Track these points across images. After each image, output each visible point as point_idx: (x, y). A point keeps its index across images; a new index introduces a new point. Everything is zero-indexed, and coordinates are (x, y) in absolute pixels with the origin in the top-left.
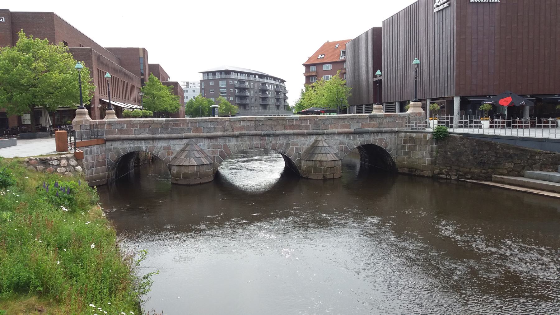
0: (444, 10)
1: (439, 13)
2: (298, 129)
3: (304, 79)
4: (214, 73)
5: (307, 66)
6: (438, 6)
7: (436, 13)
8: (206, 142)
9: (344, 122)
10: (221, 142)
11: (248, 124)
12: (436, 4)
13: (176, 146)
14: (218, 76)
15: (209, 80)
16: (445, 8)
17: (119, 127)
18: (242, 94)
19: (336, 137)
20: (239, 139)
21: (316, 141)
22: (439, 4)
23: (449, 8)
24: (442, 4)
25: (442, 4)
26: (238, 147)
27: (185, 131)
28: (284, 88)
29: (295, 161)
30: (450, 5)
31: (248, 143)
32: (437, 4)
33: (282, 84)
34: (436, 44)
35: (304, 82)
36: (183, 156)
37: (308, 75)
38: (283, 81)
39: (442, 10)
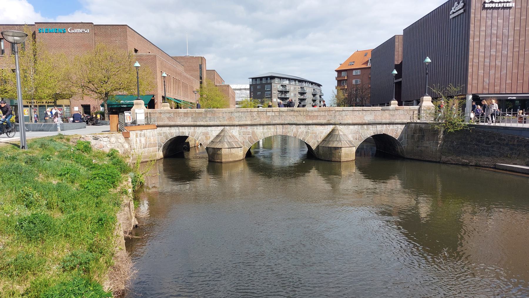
0: (459, 17)
1: (454, 19)
2: (317, 119)
3: (336, 83)
4: (261, 78)
5: (339, 72)
6: (454, 13)
7: (452, 20)
8: (237, 128)
9: (359, 114)
10: (249, 129)
11: (273, 114)
12: (452, 11)
13: (213, 132)
14: (264, 81)
15: (257, 85)
16: (460, 14)
17: (168, 115)
18: (283, 96)
19: (351, 127)
20: (266, 127)
21: (333, 131)
22: (454, 11)
23: (464, 14)
24: (457, 11)
25: (457, 11)
26: (264, 134)
27: (221, 120)
28: (321, 91)
29: (314, 148)
30: (464, 11)
31: (273, 130)
32: (453, 10)
33: (318, 88)
34: (451, 47)
35: (336, 85)
36: (218, 140)
37: (340, 79)
38: (319, 85)
39: (458, 16)
